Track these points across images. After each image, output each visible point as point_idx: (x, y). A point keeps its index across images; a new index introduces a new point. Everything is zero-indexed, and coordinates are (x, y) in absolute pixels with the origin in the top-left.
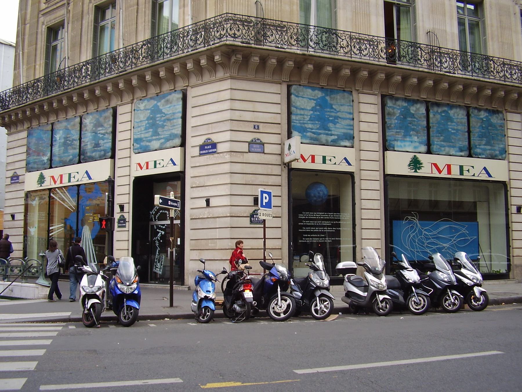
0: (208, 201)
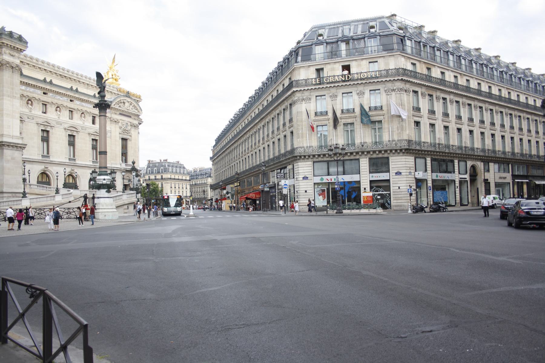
0: (399, 188)
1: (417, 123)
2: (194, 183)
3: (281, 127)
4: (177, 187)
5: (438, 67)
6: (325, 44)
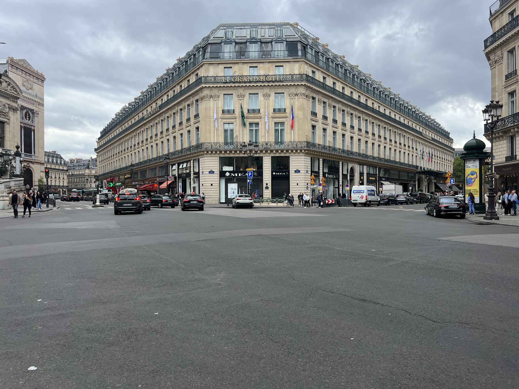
1: (314, 127)
2: (70, 174)
3: (184, 122)
4: (57, 178)
5: (332, 77)
6: (234, 44)
